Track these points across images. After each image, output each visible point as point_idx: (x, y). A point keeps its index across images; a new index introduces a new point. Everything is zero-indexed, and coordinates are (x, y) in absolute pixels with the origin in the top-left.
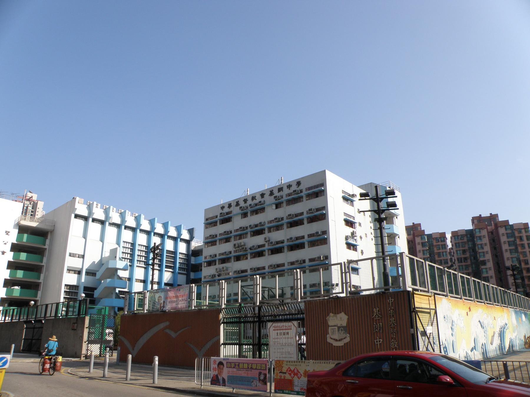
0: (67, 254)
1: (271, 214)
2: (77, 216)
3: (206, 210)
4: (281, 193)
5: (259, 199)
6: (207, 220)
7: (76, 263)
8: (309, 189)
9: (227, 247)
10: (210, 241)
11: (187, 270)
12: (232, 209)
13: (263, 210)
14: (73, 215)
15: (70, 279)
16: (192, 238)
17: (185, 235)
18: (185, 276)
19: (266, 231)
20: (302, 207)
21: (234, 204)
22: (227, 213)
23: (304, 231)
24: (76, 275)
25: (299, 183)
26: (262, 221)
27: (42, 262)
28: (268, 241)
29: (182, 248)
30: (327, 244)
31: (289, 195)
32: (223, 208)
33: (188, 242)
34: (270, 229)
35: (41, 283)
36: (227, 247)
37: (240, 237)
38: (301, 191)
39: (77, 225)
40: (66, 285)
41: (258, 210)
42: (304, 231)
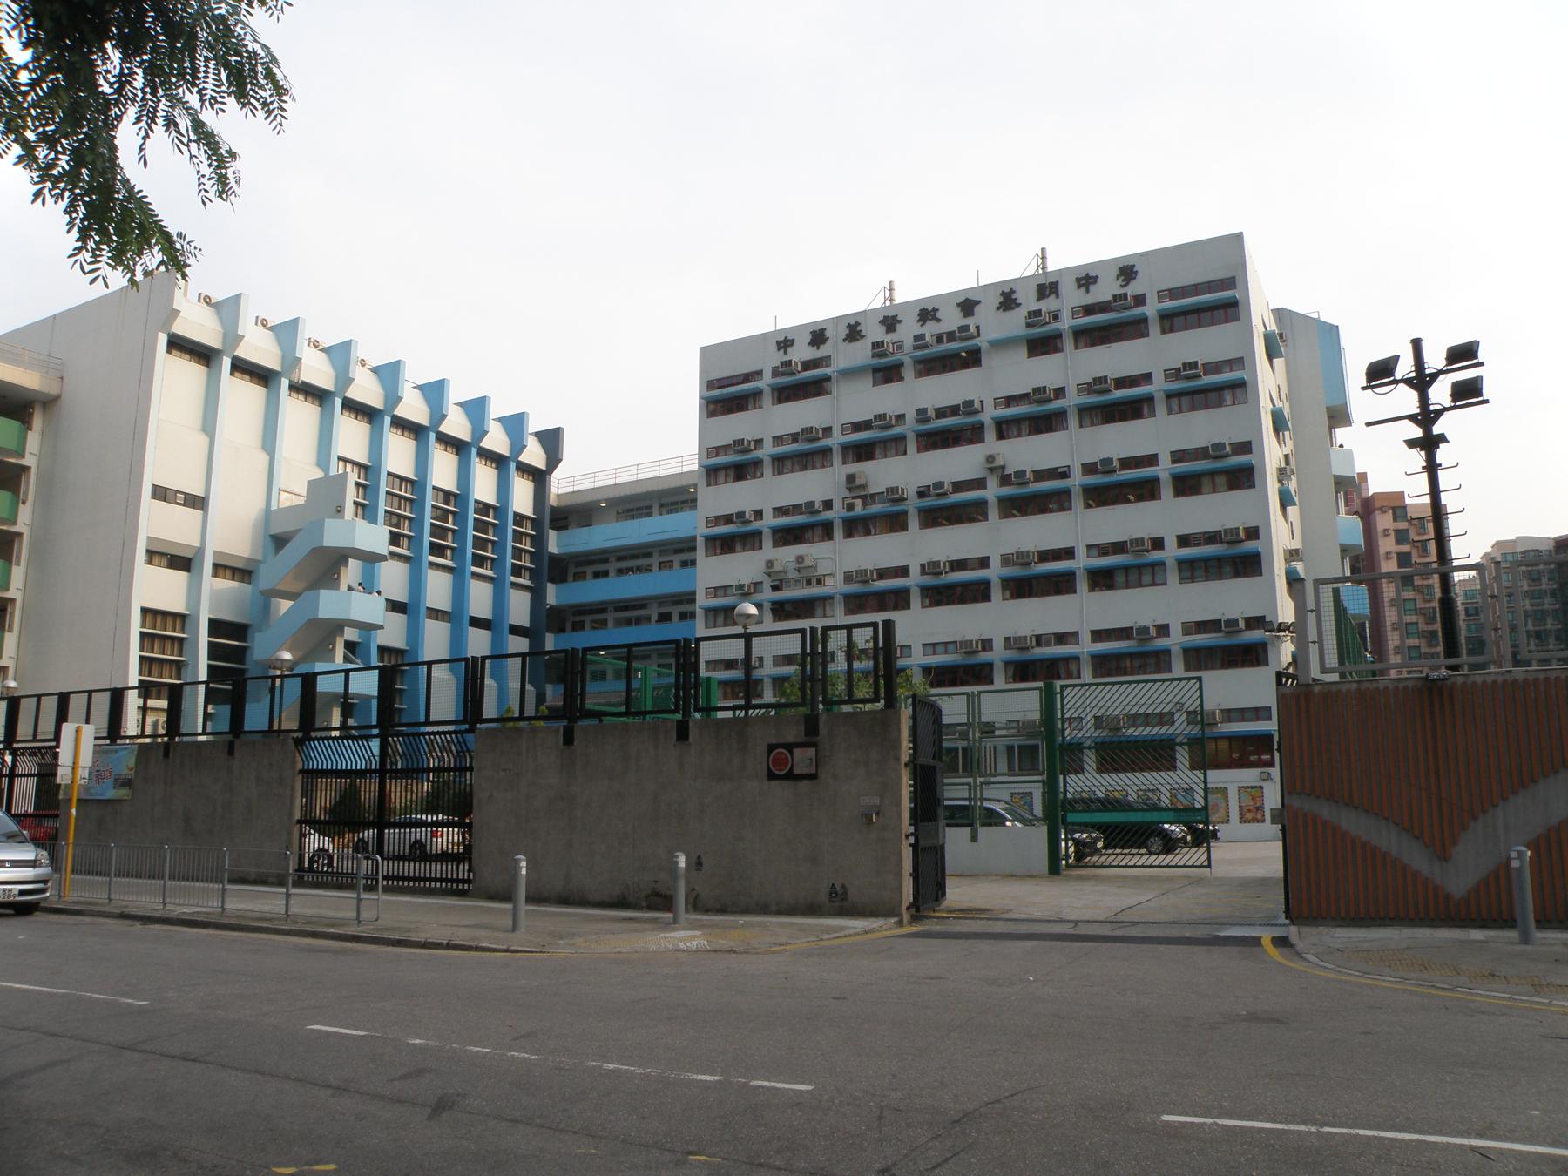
0: (147, 491)
1: (1009, 375)
2: (178, 344)
3: (704, 351)
4: (1049, 304)
5: (951, 320)
6: (711, 385)
7: (175, 526)
8: (1173, 293)
9: (813, 486)
10: (727, 465)
11: (534, 575)
12: (824, 351)
13: (972, 359)
14: (163, 339)
15: (160, 588)
16: (554, 459)
17: (534, 455)
18: (527, 596)
19: (990, 434)
20: (1150, 357)
21: (836, 335)
22: (808, 365)
23: (1159, 436)
24: (181, 576)
25: (1127, 271)
26: (974, 396)
27: (15, 523)
28: (993, 467)
29: (522, 497)
30: (1253, 486)
31: (1089, 310)
32: (785, 343)
33: (539, 478)
34: (1004, 429)
35: (13, 601)
36: (813, 486)
37: (863, 452)
38: (1140, 300)
39: (177, 380)
40: (145, 611)
41: (960, 356)
42: (1159, 436)
